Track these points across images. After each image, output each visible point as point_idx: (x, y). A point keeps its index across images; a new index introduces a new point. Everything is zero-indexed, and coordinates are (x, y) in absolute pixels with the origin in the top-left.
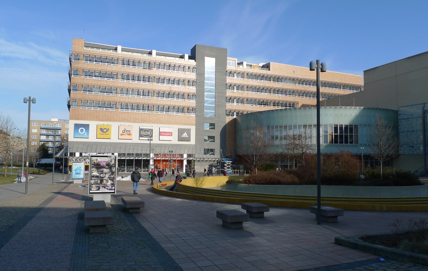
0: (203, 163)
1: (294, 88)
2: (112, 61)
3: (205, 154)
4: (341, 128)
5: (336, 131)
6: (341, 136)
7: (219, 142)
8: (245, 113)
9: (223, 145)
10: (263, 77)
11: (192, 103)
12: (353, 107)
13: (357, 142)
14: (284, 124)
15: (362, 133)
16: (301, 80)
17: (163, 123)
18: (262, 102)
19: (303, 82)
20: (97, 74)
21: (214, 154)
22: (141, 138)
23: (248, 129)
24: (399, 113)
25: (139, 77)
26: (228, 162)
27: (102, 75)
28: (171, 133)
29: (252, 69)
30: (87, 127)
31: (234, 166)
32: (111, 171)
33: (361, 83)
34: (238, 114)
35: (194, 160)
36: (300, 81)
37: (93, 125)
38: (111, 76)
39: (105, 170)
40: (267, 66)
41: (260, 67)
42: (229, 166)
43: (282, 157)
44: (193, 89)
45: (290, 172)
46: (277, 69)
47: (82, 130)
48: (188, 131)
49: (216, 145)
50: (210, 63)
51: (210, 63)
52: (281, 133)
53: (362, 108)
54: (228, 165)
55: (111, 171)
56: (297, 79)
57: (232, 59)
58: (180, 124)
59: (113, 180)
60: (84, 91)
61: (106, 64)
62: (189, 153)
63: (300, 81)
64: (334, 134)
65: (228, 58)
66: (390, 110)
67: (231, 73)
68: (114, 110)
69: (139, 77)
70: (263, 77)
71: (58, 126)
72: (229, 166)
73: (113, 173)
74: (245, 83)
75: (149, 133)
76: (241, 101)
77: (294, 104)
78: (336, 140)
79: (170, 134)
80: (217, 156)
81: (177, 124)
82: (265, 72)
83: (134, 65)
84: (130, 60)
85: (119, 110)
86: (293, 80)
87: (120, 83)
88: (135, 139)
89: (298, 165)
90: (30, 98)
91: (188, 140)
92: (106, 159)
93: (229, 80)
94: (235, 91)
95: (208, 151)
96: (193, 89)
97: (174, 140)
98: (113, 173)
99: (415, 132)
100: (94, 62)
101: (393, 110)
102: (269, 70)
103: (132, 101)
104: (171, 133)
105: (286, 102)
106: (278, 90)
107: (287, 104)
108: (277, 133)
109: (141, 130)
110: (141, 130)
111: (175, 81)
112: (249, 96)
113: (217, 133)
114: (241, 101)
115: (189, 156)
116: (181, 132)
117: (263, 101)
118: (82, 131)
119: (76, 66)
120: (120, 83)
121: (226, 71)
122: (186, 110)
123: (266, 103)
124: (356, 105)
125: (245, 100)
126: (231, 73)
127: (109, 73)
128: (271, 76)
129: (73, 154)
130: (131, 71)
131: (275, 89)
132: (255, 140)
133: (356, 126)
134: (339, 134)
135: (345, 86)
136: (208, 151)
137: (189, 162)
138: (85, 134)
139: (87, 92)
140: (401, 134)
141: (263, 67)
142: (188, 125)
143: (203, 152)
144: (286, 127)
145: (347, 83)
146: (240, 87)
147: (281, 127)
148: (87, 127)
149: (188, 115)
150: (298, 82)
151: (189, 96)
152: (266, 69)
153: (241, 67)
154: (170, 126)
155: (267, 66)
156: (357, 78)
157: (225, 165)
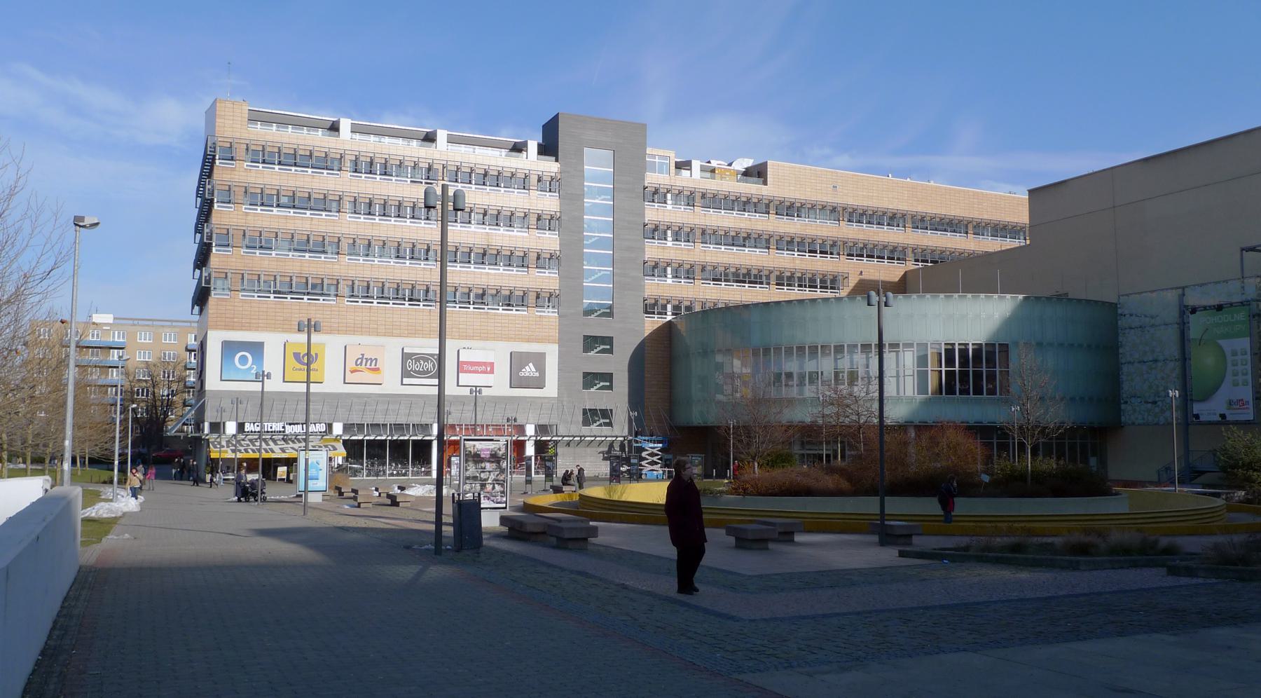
0: (578, 450)
1: (835, 234)
2: (325, 163)
3: (586, 422)
4: (963, 353)
5: (950, 361)
6: (964, 375)
7: (626, 390)
8: (698, 308)
9: (636, 399)
10: (746, 204)
11: (548, 279)
12: (996, 296)
13: (1005, 389)
14: (809, 340)
15: (1020, 360)
16: (855, 210)
17: (467, 338)
18: (744, 275)
19: (862, 215)
20: (284, 200)
21: (610, 424)
22: (406, 381)
23: (706, 352)
24: (1120, 311)
25: (399, 206)
26: (652, 447)
27: (298, 202)
28: (492, 364)
29: (717, 181)
30: (256, 349)
31: (667, 456)
32: (500, 467)
33: (1022, 216)
34: (676, 309)
35: (556, 442)
36: (851, 214)
37: (275, 344)
38: (322, 203)
39: (488, 466)
40: (758, 173)
41: (738, 172)
42: (655, 459)
43: (809, 433)
44: (549, 241)
45: (831, 471)
46: (787, 180)
47: (243, 360)
48: (539, 360)
49: (617, 399)
50: (597, 166)
51: (597, 166)
52: (801, 367)
53: (1021, 297)
54: (652, 455)
55: (500, 467)
56: (844, 209)
57: (661, 152)
58: (514, 339)
59: (502, 485)
60: (248, 247)
61: (310, 170)
62: (542, 422)
63: (851, 214)
64: (944, 369)
65: (649, 151)
66: (1096, 302)
67: (657, 195)
68: (332, 301)
69: (399, 206)
70: (746, 204)
71: (117, 339)
72: (655, 459)
73: (502, 471)
74: (697, 221)
75: (430, 365)
76: (687, 272)
77: (834, 280)
78: (949, 386)
79: (488, 368)
80: (620, 429)
81: (509, 339)
82: (752, 188)
83: (385, 174)
84: (376, 160)
85: (346, 302)
86: (834, 210)
87: (349, 224)
88: (390, 382)
89: (847, 453)
90: (309, 320)
91: (539, 383)
92: (491, 446)
93: (653, 213)
94: (670, 244)
95: (590, 416)
96: (549, 241)
97: (498, 384)
98: (502, 471)
99: (1160, 364)
100: (277, 167)
101: (1104, 303)
102: (765, 183)
103: (382, 275)
104: (492, 364)
105: (814, 275)
106: (791, 242)
107: (815, 281)
108: (792, 366)
109: (406, 357)
110: (406, 357)
111: (501, 217)
112: (708, 259)
113: (618, 364)
114: (687, 272)
115: (542, 429)
116: (518, 361)
117: (749, 271)
118: (244, 364)
119: (226, 177)
120: (349, 224)
121: (645, 188)
122: (531, 298)
123: (755, 276)
124: (1005, 290)
125: (698, 269)
126: (657, 195)
127: (317, 196)
128: (771, 201)
129: (217, 427)
130: (377, 192)
131: (781, 237)
132: (726, 386)
133: (1005, 348)
134: (957, 368)
135: (979, 228)
136: (590, 416)
137: (541, 447)
138: (251, 368)
139: (258, 252)
140: (1125, 369)
141: (747, 173)
142: (537, 340)
143: (581, 419)
144: (814, 350)
145: (985, 217)
146: (683, 234)
147: (801, 349)
148: (256, 349)
149: (536, 312)
150: (847, 215)
151: (542, 260)
152: (756, 179)
153: (685, 173)
154: (490, 344)
155: (758, 173)
156: (1013, 205)
157: (644, 454)
